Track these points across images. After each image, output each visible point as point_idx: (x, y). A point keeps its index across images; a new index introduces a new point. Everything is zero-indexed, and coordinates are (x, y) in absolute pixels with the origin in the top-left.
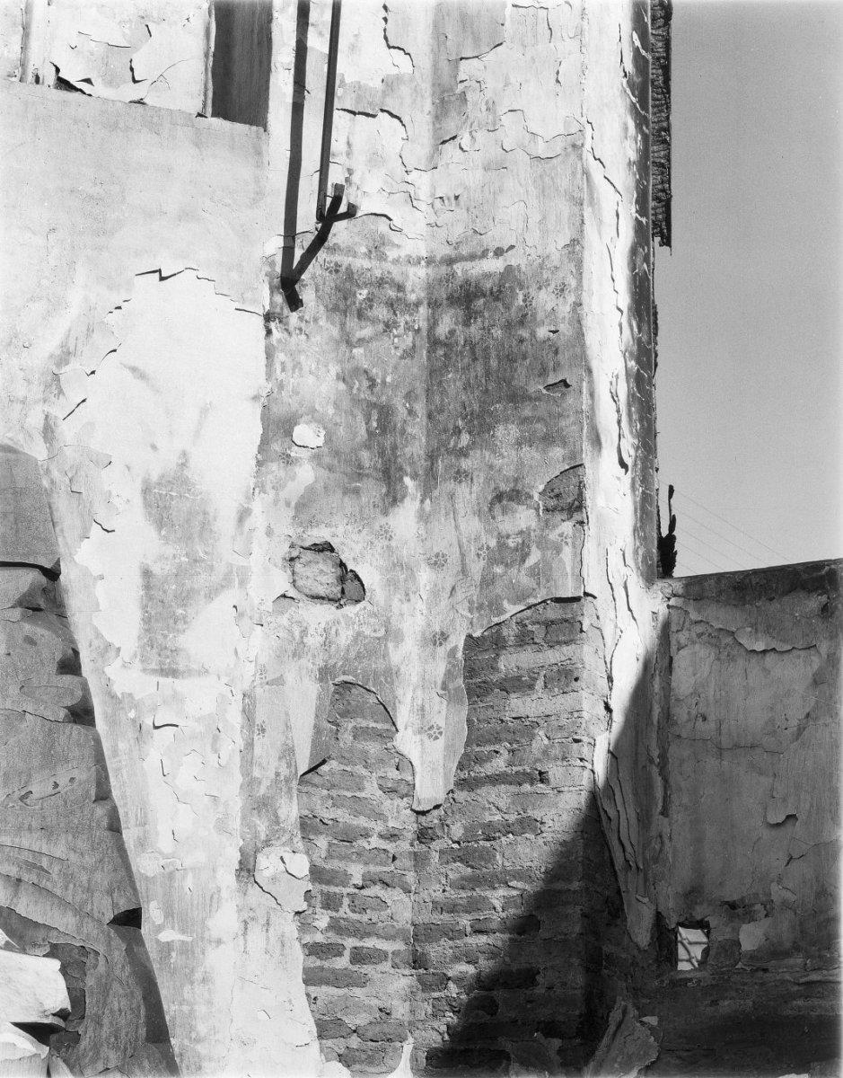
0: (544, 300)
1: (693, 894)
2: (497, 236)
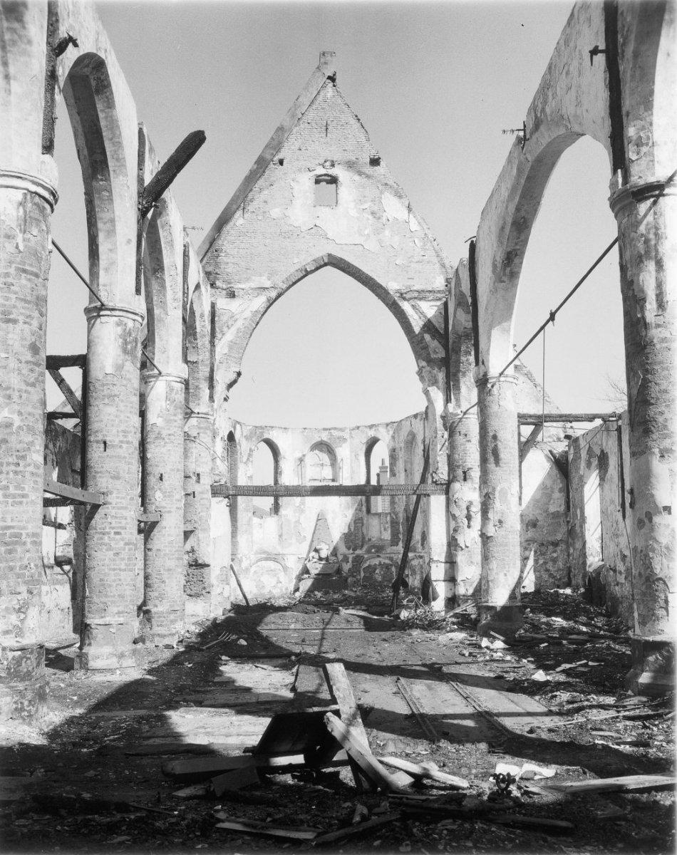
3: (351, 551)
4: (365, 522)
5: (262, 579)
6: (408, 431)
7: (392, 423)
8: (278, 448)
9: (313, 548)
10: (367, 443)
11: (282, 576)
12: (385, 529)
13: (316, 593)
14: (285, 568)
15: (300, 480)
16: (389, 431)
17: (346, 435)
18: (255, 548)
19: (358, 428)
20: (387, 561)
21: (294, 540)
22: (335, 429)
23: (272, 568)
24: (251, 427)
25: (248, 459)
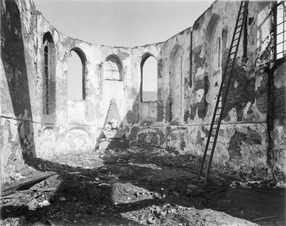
0: (136, 90)
1: (143, 116)
2: (134, 86)
3: (131, 124)
4: (140, 107)
5: (74, 141)
6: (174, 45)
7: (159, 43)
8: (85, 56)
9: (108, 122)
10: (142, 57)
11: (87, 139)
12: (152, 112)
13: (110, 150)
14: (90, 134)
15: (100, 79)
16: (158, 48)
17: (129, 53)
18: (69, 120)
19: (137, 47)
20: (154, 131)
21: (95, 117)
22: (122, 47)
23: (81, 134)
24: (66, 37)
25: (64, 59)
